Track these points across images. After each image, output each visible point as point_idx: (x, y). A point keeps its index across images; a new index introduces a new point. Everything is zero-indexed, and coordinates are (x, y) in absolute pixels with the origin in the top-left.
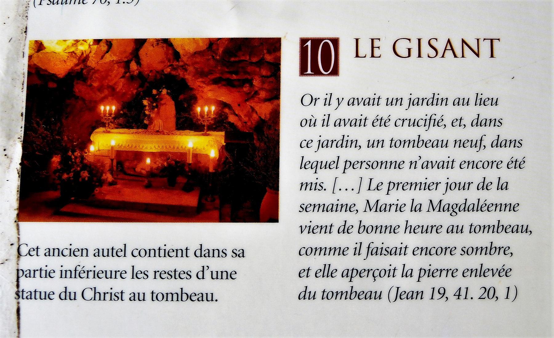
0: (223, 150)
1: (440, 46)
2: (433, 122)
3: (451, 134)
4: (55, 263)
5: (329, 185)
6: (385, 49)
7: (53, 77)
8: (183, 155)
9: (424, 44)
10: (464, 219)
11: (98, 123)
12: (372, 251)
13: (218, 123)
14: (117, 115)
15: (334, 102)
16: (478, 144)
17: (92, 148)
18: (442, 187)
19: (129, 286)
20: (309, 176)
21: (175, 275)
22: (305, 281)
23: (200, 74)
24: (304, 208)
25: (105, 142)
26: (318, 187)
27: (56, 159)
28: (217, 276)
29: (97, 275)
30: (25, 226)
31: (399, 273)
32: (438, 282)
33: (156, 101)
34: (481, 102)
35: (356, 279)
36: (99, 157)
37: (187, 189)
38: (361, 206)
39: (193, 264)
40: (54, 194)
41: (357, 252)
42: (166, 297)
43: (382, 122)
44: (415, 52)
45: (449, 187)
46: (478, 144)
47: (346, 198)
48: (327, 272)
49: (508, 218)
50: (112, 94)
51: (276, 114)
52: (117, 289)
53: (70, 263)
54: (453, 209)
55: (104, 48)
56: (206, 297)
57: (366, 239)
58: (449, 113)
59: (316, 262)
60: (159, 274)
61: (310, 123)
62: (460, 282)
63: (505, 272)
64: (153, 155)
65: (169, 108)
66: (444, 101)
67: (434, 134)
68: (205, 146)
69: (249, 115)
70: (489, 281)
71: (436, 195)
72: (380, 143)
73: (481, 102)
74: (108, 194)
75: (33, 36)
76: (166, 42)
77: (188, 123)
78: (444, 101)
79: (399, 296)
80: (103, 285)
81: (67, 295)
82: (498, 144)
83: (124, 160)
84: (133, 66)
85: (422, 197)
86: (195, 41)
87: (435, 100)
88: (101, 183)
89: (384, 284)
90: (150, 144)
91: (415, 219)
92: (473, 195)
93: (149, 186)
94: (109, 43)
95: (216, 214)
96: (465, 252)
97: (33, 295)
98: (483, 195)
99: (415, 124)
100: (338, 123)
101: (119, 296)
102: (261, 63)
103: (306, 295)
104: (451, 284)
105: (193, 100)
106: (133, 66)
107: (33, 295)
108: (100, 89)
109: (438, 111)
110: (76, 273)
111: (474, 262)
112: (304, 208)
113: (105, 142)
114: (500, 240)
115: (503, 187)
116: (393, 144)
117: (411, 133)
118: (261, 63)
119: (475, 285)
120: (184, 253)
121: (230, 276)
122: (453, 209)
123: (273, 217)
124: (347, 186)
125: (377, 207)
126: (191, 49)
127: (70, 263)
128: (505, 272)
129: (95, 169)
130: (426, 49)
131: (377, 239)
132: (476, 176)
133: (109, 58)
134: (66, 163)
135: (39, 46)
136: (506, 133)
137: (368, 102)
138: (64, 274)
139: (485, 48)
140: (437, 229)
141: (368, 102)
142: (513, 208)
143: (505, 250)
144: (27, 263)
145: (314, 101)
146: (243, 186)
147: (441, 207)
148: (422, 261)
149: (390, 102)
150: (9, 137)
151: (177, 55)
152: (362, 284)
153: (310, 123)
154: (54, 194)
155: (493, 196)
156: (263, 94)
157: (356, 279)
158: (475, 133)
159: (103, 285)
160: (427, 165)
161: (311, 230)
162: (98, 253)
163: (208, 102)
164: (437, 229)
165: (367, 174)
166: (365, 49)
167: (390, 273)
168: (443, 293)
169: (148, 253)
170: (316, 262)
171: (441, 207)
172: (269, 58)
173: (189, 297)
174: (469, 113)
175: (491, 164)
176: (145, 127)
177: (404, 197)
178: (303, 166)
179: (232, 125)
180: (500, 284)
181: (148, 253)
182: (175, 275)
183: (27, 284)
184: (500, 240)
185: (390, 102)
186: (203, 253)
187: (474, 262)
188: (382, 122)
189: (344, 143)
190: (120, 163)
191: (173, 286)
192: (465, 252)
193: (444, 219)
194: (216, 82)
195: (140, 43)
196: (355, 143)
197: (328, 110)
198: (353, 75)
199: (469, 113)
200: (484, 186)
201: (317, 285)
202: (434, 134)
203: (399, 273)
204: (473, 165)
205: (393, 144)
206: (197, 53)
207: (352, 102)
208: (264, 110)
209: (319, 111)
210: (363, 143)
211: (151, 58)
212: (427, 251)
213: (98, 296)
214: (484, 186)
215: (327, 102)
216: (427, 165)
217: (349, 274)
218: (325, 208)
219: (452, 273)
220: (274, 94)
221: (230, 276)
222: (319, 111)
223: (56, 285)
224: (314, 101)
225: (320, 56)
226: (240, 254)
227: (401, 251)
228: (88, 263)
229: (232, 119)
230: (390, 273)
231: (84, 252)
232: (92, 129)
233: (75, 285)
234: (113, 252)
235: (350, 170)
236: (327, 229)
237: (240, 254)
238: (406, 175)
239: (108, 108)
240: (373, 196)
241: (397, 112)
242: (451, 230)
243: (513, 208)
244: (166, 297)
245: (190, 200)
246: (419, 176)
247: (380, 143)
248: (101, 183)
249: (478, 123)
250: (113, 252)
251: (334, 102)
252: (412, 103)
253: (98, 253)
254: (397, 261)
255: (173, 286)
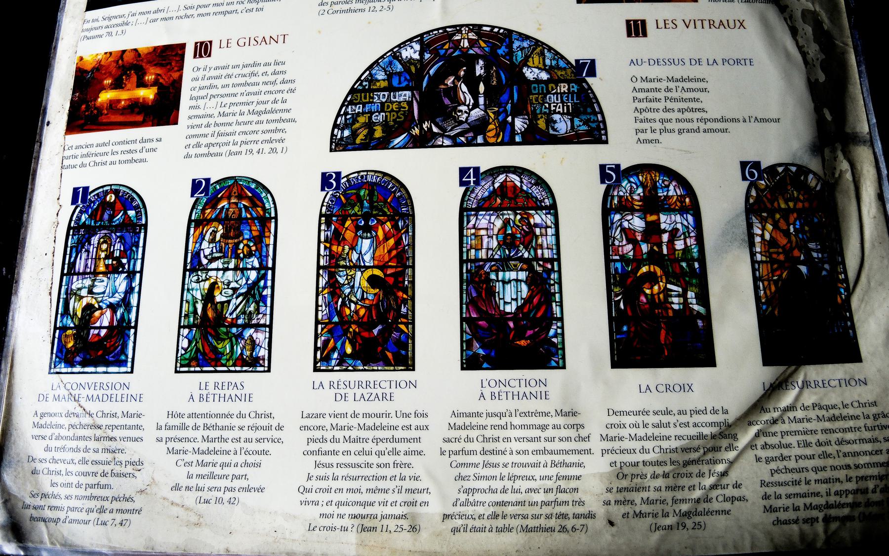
0: (156, 95)
1: (259, 40)
2: (253, 74)
3: (260, 79)
4: (79, 152)
5: (202, 106)
6: (233, 43)
7: (87, 72)
8: (138, 99)
9: (252, 40)
10: (264, 117)
11: (103, 88)
12: (220, 134)
13: (155, 83)
14: (112, 84)
15: (208, 69)
16: (274, 83)
17: (100, 100)
18: (255, 104)
19: (110, 158)
20: (193, 103)
21: (130, 152)
22: (188, 150)
23: (149, 62)
24: (190, 118)
25: (105, 96)
26: (198, 107)
27: (83, 106)
28: (148, 151)
29: (96, 155)
30: (69, 137)
31: (398, 478)
32: (249, 147)
33: (129, 76)
34: (277, 63)
35: (211, 148)
36: (102, 104)
37: (139, 113)
38: (216, 114)
39: (138, 146)
40: (81, 122)
41: (213, 135)
42: (125, 162)
43: (229, 76)
44: (247, 44)
45: (258, 103)
46: (274, 83)
47: (209, 112)
48: (198, 145)
49: (285, 116)
50: (110, 75)
51: (181, 77)
52: (104, 161)
53: (85, 151)
54: (259, 113)
55: (108, 55)
56: (143, 161)
57: (217, 129)
58: (261, 70)
59: (193, 141)
60: (123, 152)
61: (197, 79)
62: (260, 146)
63: (282, 141)
64: (125, 100)
65: (134, 79)
66: (259, 64)
67: (253, 79)
68: (148, 94)
69: (169, 78)
70: (273, 145)
71: (251, 108)
72: (228, 86)
73: (277, 63)
74: (104, 120)
75: (79, 54)
76: (136, 50)
77: (141, 84)
78: (259, 64)
79: (230, 154)
80: (98, 159)
81: (83, 165)
82: (283, 82)
83: (113, 103)
84: (120, 62)
85: (245, 109)
86: (148, 48)
87: (255, 65)
88: (102, 114)
89: (224, 149)
90: (124, 95)
91: (241, 119)
92: (269, 107)
93: (122, 114)
94: (111, 53)
95: (156, 121)
96: (263, 132)
97: (68, 167)
98: (275, 106)
99: (245, 76)
100: (209, 79)
101: (105, 164)
102: (176, 55)
103: (188, 156)
104: (255, 148)
105: (145, 74)
106: (120, 62)
107: (68, 167)
108: (105, 74)
109: (256, 69)
110: (88, 155)
111: (267, 136)
112: (190, 118)
113: (105, 96)
114: (281, 126)
115: (284, 101)
116: (234, 85)
117: (242, 80)
118: (176, 55)
119: (267, 147)
120: (135, 141)
121: (154, 150)
122: (259, 113)
123: (176, 123)
124: (211, 106)
125: (224, 115)
126: (146, 52)
127: (85, 151)
128: (282, 141)
129: (100, 109)
130: (253, 42)
131: (222, 129)
132: (271, 98)
133: (110, 60)
134: (88, 107)
135: (81, 59)
136: (287, 77)
137: (223, 68)
138: (82, 156)
139: (281, 39)
140: (251, 123)
141: (223, 68)
142: (288, 111)
143: (283, 131)
144: (68, 153)
145: (199, 69)
146: (164, 110)
147: (253, 113)
148: (243, 138)
149: (234, 67)
150: (65, 100)
151: (139, 55)
152: (213, 150)
153: (197, 79)
154: (81, 122)
155: (279, 106)
156: (176, 69)
157: (211, 148)
158: (272, 78)
159: (98, 159)
160: (248, 94)
161: (193, 127)
162: (98, 145)
163: (151, 74)
164: (251, 123)
165: (219, 100)
166: (224, 44)
167: (227, 144)
168: (251, 152)
169: (119, 143)
170: (193, 141)
171: (253, 113)
172: (179, 52)
173: (135, 161)
174: (270, 69)
175: (279, 91)
176: (123, 88)
177: (236, 109)
178: (191, 99)
179: (161, 84)
180: (279, 146)
181: (119, 143)
182: (130, 152)
183: (66, 163)
184: (281, 126)
185: (234, 67)
186: (143, 141)
187: (267, 136)
188: (229, 76)
189: (211, 87)
190: (111, 105)
191: (129, 157)
192: (263, 132)
193: (255, 118)
194: (156, 65)
195: (124, 52)
196: (216, 87)
197: (205, 73)
198: (218, 55)
199: (270, 69)
200: (275, 102)
201: (193, 151)
202: (253, 79)
203: (398, 478)
204: (271, 92)
205: (234, 85)
206: (149, 53)
207: (215, 69)
208: (175, 75)
209: (200, 74)
210: (219, 86)
211: (128, 57)
212: (245, 133)
213: (96, 164)
214: (275, 102)
215: (205, 69)
216: (248, 94)
217: (208, 146)
218: (199, 117)
219: (256, 142)
220: (181, 68)
221: (154, 150)
222: (200, 74)
223: (78, 161)
224: (199, 69)
225: (203, 49)
226: (159, 140)
227: (233, 134)
228: (93, 150)
229: (161, 81)
230: (227, 144)
231: (92, 145)
232: (100, 92)
233: (86, 160)
234: (104, 144)
235: (213, 99)
236: (200, 126)
237: (159, 140)
238: (239, 99)
239: (108, 82)
240: (222, 110)
241: (237, 71)
242: (257, 123)
243: (288, 111)
244: (125, 162)
245: (140, 118)
246: (244, 99)
247: (228, 86)
248: (102, 114)
249: (274, 73)
250: (104, 144)
251: (208, 69)
252: (244, 66)
253: (98, 145)
254: (230, 139)
255: (129, 157)
